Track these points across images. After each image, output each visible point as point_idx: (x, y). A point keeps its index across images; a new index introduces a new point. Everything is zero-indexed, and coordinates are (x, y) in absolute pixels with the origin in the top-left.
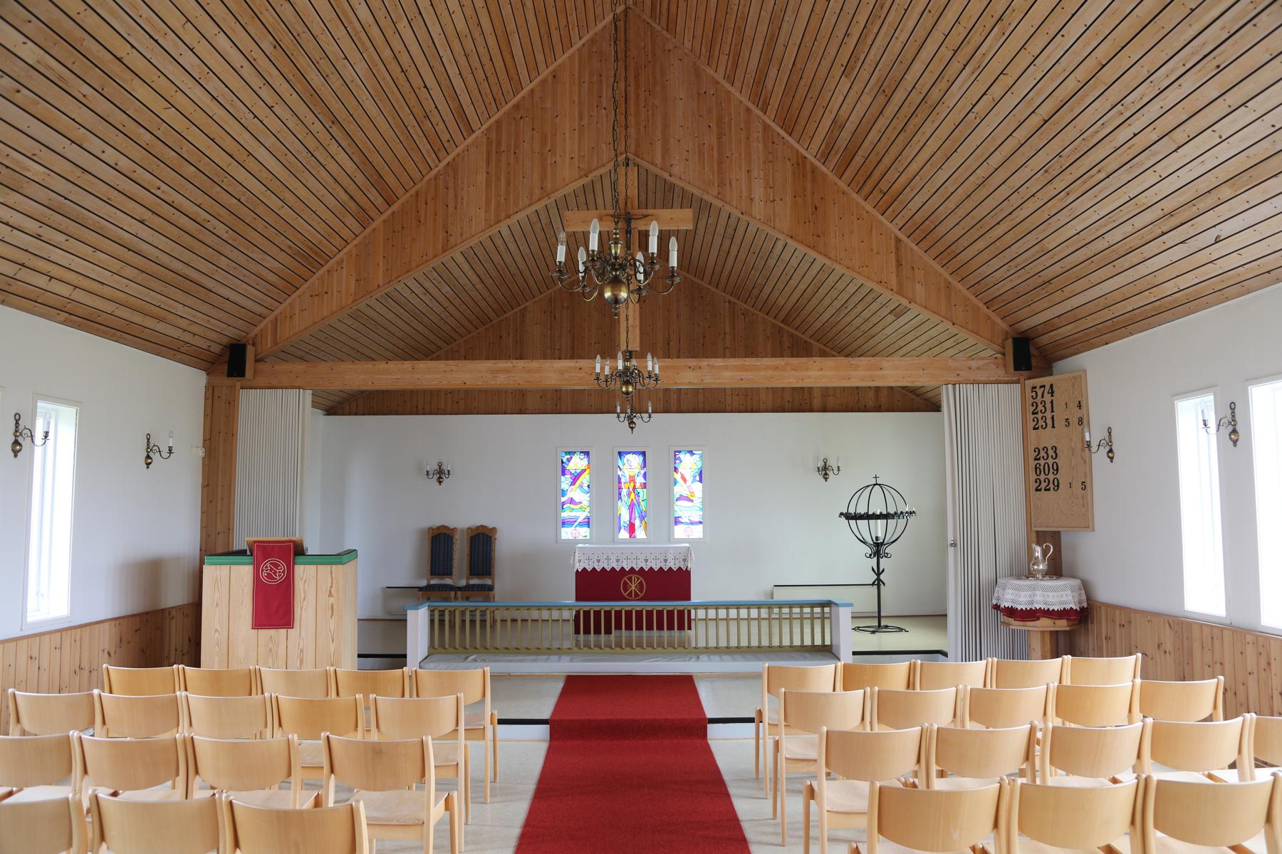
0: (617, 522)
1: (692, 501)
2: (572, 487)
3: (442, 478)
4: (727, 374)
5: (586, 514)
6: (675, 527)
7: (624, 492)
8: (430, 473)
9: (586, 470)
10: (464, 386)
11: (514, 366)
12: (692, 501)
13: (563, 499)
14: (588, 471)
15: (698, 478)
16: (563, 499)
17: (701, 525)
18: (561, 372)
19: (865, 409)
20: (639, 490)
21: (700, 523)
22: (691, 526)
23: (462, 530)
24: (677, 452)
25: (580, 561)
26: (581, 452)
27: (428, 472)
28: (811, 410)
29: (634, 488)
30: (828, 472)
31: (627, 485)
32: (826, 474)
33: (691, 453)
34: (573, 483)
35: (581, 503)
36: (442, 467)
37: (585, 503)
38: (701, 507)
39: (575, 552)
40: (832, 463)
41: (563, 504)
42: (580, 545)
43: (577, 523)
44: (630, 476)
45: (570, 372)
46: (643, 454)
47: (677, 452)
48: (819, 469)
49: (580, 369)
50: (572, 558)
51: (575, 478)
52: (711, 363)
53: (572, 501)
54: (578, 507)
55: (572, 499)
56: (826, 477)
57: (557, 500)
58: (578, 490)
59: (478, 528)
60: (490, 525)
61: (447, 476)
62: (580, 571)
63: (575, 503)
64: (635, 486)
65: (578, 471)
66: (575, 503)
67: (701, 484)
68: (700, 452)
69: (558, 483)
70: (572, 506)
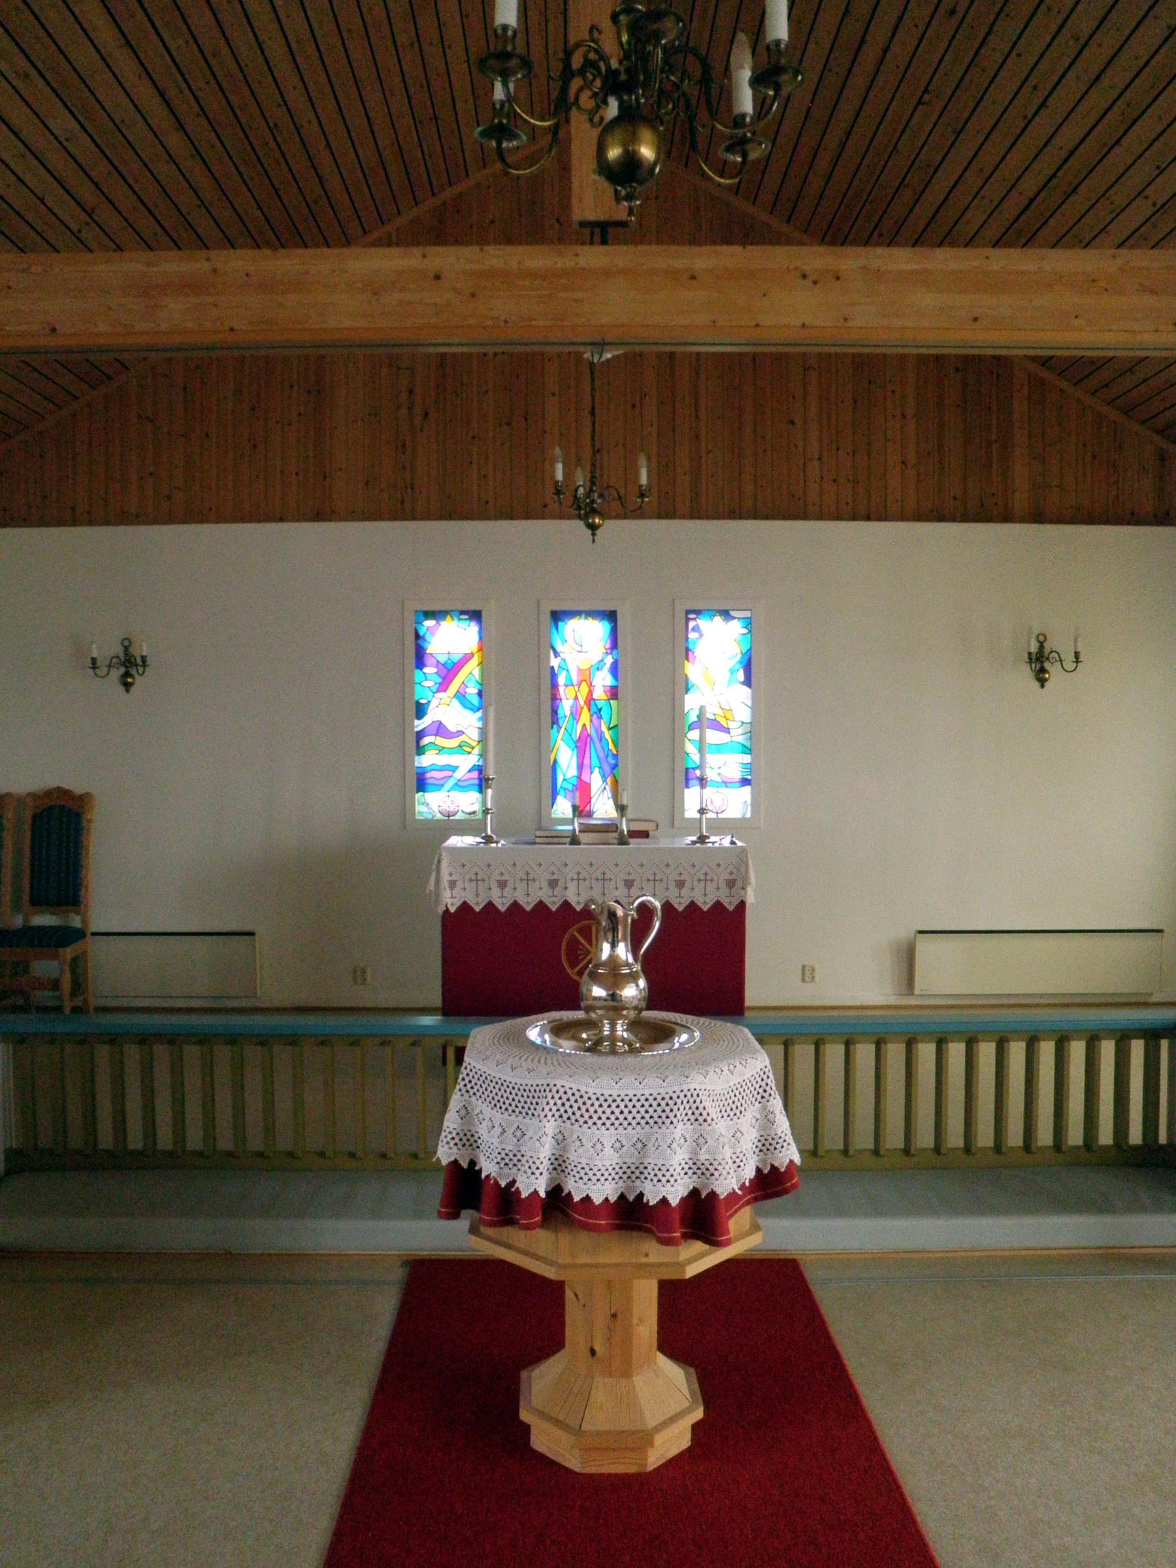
0: (547, 782)
1: (727, 730)
2: (441, 695)
3: (131, 676)
4: (927, 299)
5: (473, 759)
6: (686, 790)
7: (565, 707)
8: (99, 664)
9: (472, 655)
10: (52, 342)
11: (215, 270)
12: (727, 730)
13: (420, 725)
14: (475, 661)
15: (741, 676)
16: (420, 725)
17: (748, 789)
18: (374, 288)
19: (1134, 519)
20: (600, 704)
21: (745, 782)
22: (724, 790)
23: (20, 800)
24: (694, 612)
25: (452, 884)
26: (462, 612)
27: (94, 660)
28: (1006, 517)
29: (590, 700)
30: (1047, 665)
31: (571, 692)
32: (1043, 670)
33: (726, 614)
34: (443, 686)
35: (460, 733)
36: (130, 649)
37: (473, 735)
38: (748, 744)
39: (439, 862)
40: (1060, 643)
41: (420, 735)
42: (455, 841)
43: (451, 782)
44: (580, 671)
45: (403, 289)
46: (611, 616)
47: (694, 612)
48: (1030, 659)
49: (438, 277)
50: (434, 875)
51: (448, 673)
52: (875, 264)
53: (440, 729)
54: (454, 742)
55: (440, 722)
56: (1041, 677)
57: (405, 725)
58: (456, 702)
59: (49, 793)
60: (77, 786)
61: (141, 670)
62: (452, 910)
63: (448, 735)
64: (590, 693)
65: (456, 658)
66: (448, 735)
67: (747, 691)
68: (748, 614)
69: (406, 685)
70: (440, 741)
